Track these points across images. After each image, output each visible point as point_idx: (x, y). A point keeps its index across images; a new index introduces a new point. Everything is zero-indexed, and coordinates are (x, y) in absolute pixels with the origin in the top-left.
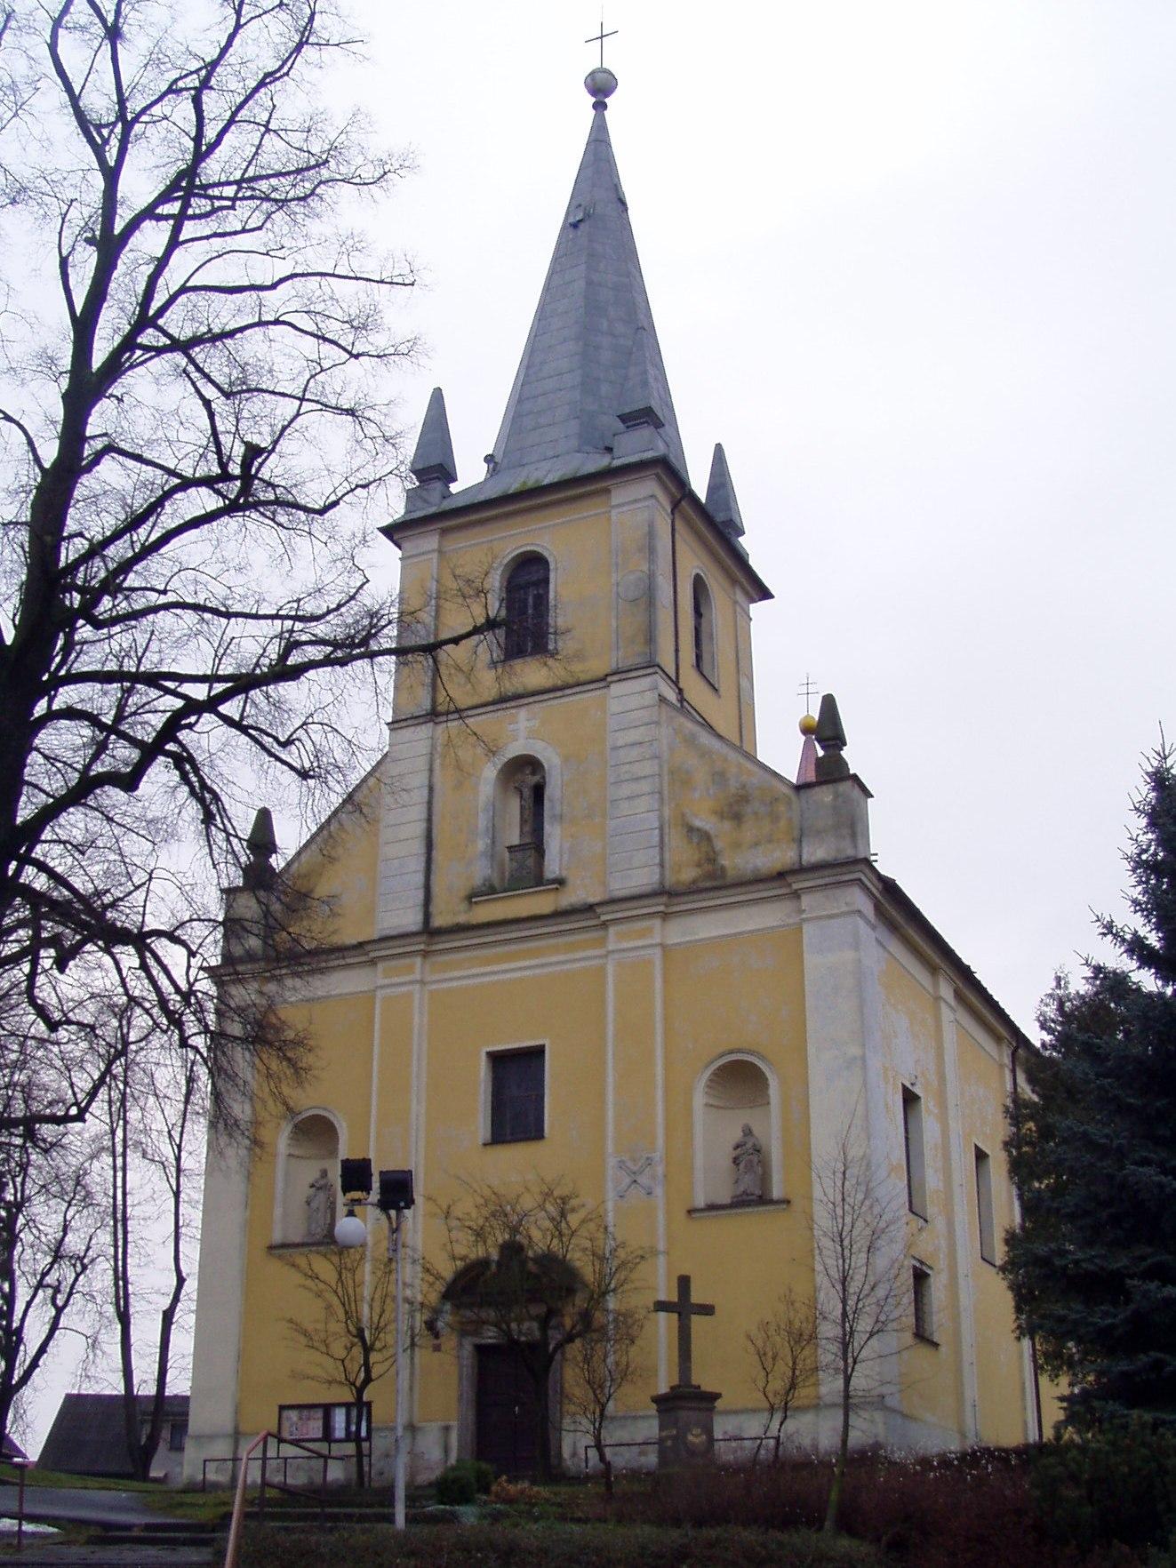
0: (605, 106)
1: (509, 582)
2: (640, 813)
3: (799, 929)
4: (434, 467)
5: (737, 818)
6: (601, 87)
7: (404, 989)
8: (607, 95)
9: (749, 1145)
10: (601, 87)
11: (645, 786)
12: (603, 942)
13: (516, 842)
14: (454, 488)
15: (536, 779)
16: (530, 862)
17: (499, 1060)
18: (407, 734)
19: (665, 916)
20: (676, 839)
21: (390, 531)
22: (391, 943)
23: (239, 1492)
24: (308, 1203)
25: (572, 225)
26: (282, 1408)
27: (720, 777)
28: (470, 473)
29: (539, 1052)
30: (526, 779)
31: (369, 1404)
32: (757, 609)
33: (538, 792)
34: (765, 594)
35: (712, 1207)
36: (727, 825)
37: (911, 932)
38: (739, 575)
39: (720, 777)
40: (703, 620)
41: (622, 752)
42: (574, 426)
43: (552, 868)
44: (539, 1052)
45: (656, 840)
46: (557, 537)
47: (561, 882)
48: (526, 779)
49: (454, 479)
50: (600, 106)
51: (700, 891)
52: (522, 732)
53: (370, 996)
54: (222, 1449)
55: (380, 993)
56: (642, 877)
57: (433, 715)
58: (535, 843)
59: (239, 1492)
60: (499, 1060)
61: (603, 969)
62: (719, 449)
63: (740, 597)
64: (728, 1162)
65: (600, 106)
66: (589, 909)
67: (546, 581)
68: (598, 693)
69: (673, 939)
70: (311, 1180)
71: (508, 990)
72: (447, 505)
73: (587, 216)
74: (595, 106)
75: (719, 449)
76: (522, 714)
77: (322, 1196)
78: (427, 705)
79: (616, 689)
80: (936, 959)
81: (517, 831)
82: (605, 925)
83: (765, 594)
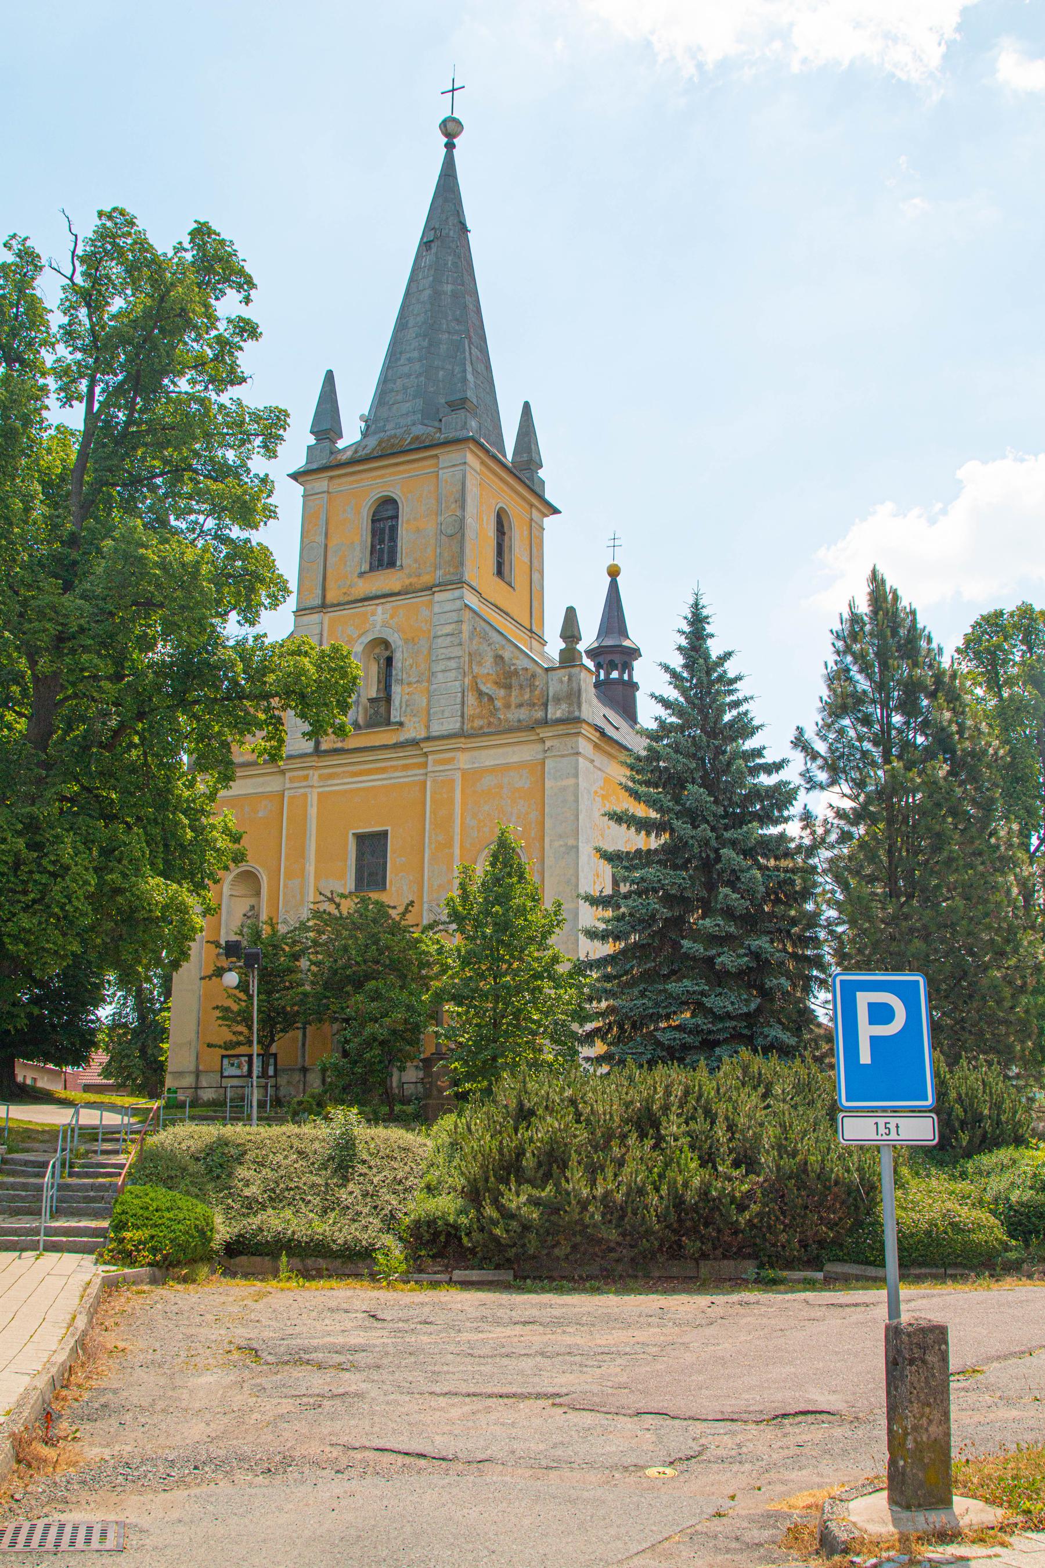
0: (454, 147)
2: (449, 682)
5: (509, 687)
6: (451, 129)
7: (302, 790)
8: (455, 137)
10: (451, 129)
11: (453, 664)
13: (374, 695)
14: (341, 444)
15: (387, 653)
16: (382, 710)
17: (361, 839)
18: (306, 619)
20: (471, 699)
21: (295, 476)
23: (734, 712)
25: (426, 245)
27: (499, 658)
28: (351, 434)
29: (384, 834)
31: (275, 1055)
32: (549, 522)
33: (389, 661)
34: (556, 511)
36: (502, 692)
39: (499, 658)
40: (506, 538)
41: (439, 640)
42: (419, 403)
43: (395, 716)
44: (384, 834)
45: (459, 700)
46: (405, 483)
47: (401, 724)
49: (341, 437)
50: (450, 146)
51: (485, 734)
54: (188, 1081)
56: (452, 725)
57: (324, 606)
58: (386, 697)
59: (734, 712)
60: (361, 839)
62: (527, 406)
63: (535, 514)
65: (450, 146)
66: (415, 743)
70: (243, 911)
73: (436, 238)
74: (446, 146)
75: (527, 406)
76: (380, 609)
78: (318, 601)
79: (438, 597)
81: (375, 689)
83: (556, 511)
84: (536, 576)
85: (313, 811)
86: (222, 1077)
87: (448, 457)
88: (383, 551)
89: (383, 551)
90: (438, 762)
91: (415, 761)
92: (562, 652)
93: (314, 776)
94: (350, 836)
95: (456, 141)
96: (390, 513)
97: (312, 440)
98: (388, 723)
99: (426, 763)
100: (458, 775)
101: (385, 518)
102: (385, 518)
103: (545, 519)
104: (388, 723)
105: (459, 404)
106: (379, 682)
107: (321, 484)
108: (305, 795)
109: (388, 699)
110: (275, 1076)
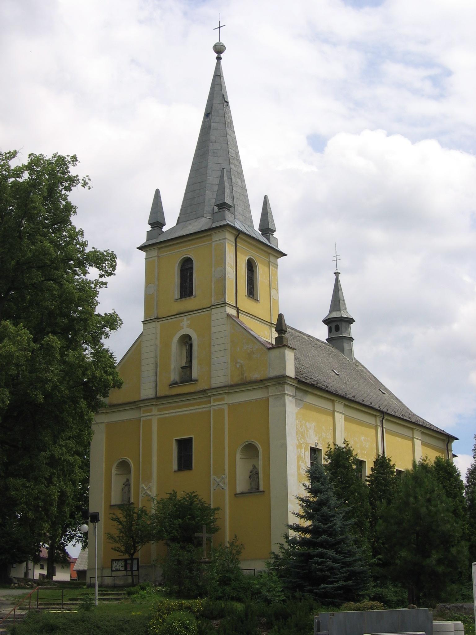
1: (181, 268)
3: (267, 400)
4: (157, 222)
9: (254, 472)
10: (219, 49)
12: (209, 402)
14: (165, 229)
16: (188, 373)
19: (228, 393)
21: (141, 248)
22: (143, 402)
24: (122, 490)
26: (113, 560)
28: (170, 222)
29: (191, 439)
30: (186, 340)
35: (242, 493)
37: (317, 392)
38: (269, 251)
44: (191, 439)
48: (186, 340)
49: (164, 225)
50: (219, 59)
52: (185, 327)
53: (139, 420)
55: (142, 419)
58: (188, 367)
61: (210, 411)
64: (248, 477)
65: (219, 59)
66: (204, 391)
67: (192, 268)
68: (209, 312)
69: (231, 401)
71: (183, 418)
72: (162, 239)
76: (185, 318)
77: (127, 488)
79: (214, 311)
80: (332, 398)
82: (210, 396)
83: (284, 255)
84: (273, 292)
85: (155, 428)
86: (112, 571)
87: (216, 237)
88: (186, 289)
89: (186, 289)
90: (215, 401)
91: (205, 400)
92: (276, 339)
93: (155, 411)
94: (174, 442)
95: (222, 55)
96: (189, 266)
97: (149, 228)
98: (191, 380)
99: (210, 401)
100: (226, 407)
101: (187, 268)
102: (187, 268)
103: (278, 259)
104: (191, 380)
105: (223, 206)
106: (187, 357)
107: (154, 253)
108: (151, 420)
109: (190, 367)
110: (138, 570)
